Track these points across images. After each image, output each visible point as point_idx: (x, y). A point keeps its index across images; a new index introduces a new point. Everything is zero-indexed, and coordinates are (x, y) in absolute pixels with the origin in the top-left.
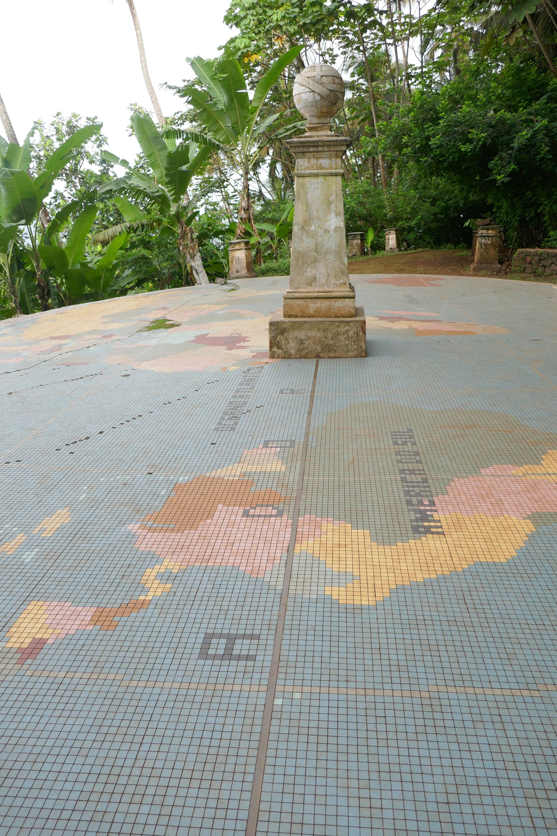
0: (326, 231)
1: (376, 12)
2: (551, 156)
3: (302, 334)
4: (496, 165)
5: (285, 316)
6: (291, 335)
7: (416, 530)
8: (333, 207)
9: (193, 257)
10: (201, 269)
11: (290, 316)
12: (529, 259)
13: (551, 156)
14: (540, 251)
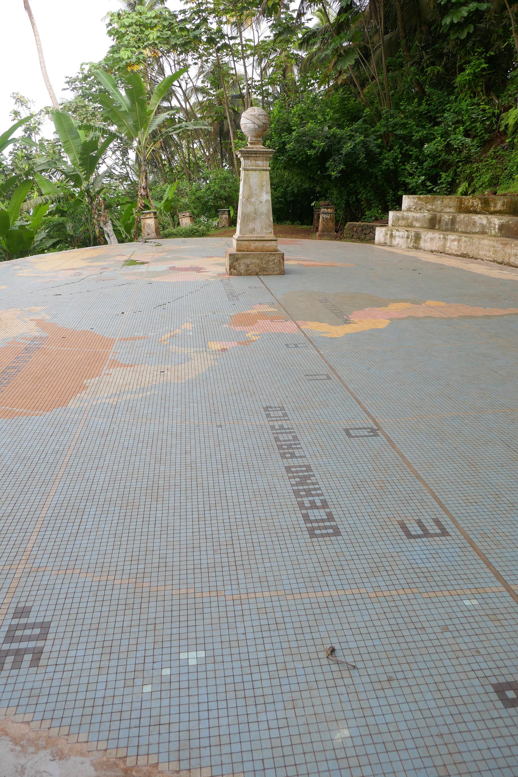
0: (261, 202)
1: (226, 37)
2: (366, 161)
3: (248, 261)
4: (331, 165)
5: (237, 251)
6: (242, 261)
7: (346, 323)
8: (264, 188)
9: (105, 223)
10: (112, 233)
11: (240, 251)
12: (355, 229)
13: (366, 161)
14: (363, 224)
